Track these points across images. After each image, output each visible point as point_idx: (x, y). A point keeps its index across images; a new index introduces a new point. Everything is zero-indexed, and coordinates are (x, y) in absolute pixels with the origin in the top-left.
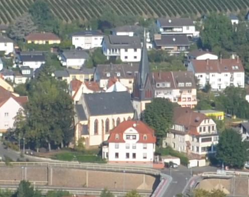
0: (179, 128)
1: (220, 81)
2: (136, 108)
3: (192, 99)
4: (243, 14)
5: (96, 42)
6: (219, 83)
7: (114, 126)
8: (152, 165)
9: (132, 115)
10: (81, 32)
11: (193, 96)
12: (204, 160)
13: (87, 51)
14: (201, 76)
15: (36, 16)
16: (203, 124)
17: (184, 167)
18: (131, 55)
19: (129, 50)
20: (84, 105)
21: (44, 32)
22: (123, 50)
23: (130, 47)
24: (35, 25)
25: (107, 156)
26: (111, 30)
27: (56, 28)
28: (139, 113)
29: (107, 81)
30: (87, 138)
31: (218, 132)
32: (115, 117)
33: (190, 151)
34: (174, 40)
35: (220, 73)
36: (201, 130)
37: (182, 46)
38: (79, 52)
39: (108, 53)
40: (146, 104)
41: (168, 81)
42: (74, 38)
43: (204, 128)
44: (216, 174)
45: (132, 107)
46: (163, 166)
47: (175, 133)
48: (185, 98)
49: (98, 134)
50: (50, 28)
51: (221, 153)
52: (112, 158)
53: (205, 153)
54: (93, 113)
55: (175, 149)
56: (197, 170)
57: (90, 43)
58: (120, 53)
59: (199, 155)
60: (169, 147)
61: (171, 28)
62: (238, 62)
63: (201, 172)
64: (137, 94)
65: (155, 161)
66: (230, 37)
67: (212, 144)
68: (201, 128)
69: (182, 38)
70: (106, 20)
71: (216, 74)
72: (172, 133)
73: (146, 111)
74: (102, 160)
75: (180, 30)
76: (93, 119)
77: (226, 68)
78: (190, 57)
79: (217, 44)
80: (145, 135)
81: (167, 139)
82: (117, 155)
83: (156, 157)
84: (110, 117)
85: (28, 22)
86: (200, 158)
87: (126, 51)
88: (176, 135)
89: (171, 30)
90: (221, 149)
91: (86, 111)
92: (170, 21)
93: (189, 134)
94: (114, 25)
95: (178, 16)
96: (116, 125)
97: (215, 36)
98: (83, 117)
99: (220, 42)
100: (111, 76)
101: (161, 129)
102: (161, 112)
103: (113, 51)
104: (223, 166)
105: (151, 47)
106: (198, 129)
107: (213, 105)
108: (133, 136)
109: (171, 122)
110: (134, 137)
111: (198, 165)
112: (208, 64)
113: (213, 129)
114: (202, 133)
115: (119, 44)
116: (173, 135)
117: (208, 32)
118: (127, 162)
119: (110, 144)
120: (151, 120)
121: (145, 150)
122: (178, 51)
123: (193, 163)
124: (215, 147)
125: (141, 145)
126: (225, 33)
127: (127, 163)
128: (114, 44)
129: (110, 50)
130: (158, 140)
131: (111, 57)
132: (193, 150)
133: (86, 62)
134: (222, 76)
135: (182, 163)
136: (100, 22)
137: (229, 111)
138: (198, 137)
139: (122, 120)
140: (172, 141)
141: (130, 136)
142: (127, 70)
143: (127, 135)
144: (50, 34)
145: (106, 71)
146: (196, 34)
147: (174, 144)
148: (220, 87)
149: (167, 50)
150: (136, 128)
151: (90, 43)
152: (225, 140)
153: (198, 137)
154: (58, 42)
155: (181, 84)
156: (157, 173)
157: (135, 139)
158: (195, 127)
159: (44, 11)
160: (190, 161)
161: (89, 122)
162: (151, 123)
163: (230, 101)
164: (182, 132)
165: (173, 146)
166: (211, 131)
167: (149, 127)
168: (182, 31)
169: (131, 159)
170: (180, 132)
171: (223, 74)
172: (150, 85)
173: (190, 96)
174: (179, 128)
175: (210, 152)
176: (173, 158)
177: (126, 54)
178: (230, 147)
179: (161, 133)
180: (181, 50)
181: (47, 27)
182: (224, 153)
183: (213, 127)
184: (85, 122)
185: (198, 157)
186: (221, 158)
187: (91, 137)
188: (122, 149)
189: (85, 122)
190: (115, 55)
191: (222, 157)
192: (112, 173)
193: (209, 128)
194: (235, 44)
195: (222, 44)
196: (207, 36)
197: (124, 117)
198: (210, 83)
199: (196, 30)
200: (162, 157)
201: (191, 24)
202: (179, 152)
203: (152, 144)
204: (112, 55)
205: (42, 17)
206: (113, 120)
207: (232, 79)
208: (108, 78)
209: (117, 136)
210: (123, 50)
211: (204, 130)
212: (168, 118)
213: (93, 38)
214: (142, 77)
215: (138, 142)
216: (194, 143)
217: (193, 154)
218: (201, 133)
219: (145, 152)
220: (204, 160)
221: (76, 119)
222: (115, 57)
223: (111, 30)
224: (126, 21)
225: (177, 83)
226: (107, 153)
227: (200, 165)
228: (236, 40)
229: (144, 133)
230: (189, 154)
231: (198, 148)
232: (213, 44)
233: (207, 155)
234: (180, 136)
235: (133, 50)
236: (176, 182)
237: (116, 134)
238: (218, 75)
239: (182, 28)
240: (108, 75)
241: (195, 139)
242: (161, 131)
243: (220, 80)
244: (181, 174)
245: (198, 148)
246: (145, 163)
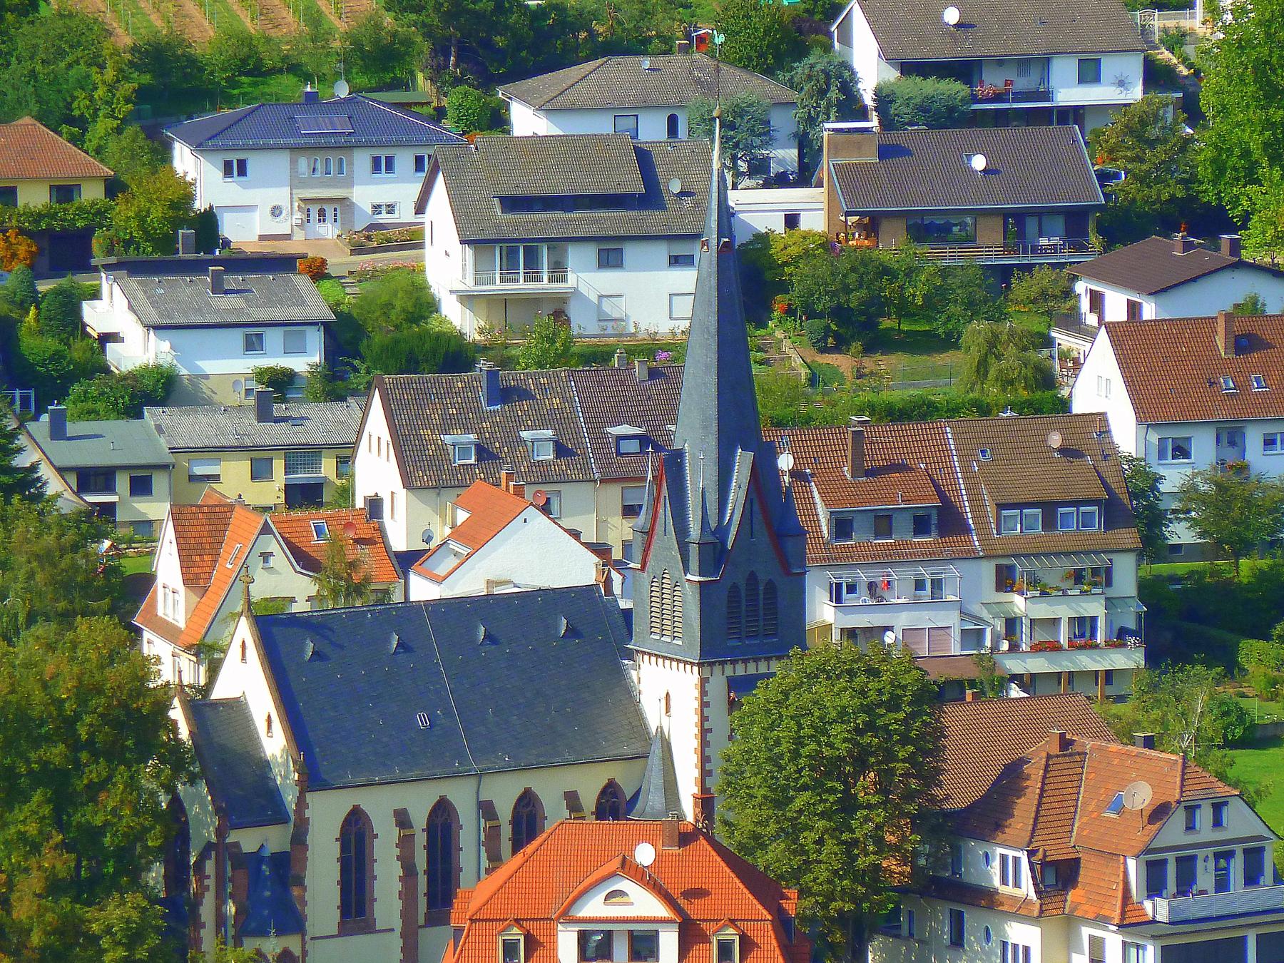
76: (326, 814)
161: (299, 839)
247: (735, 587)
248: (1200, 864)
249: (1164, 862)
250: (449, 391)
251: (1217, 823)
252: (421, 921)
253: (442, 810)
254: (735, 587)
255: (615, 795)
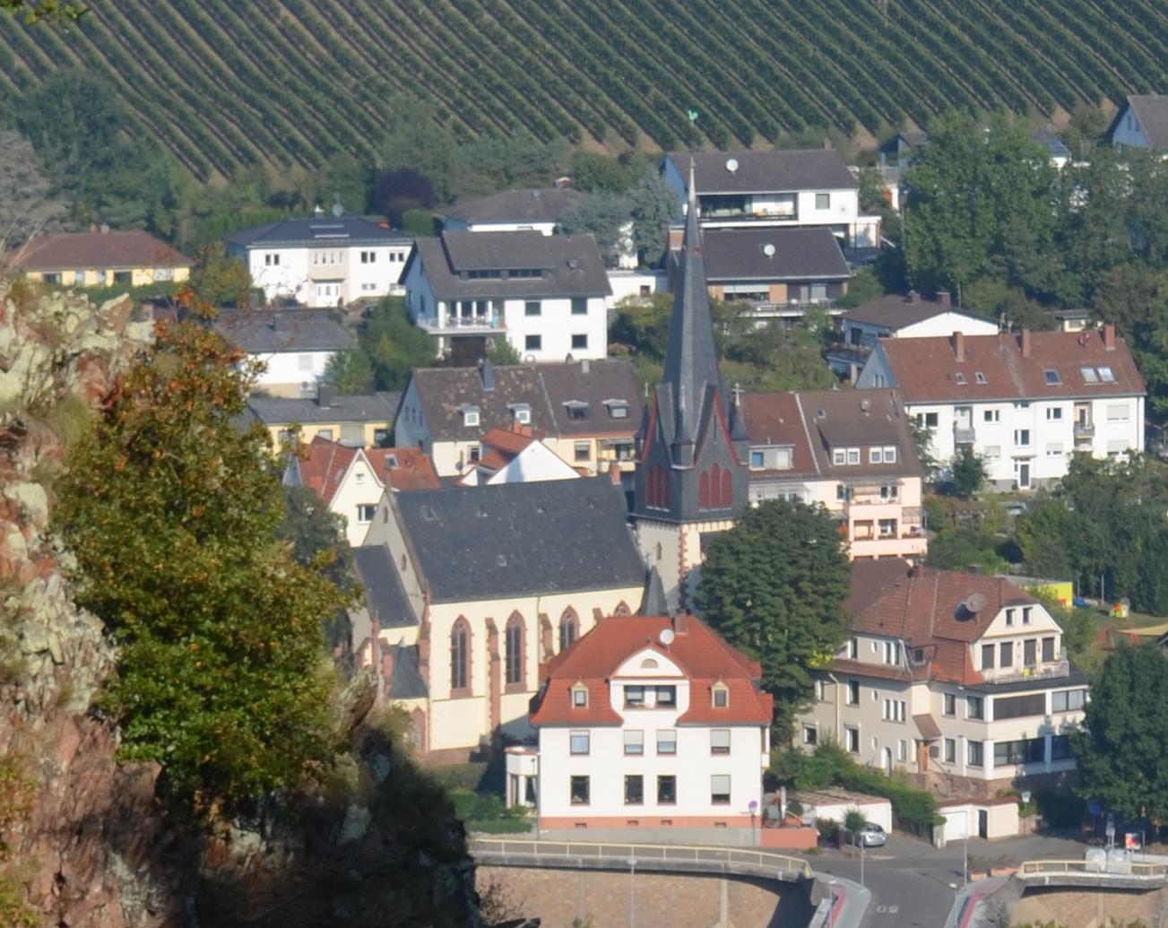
0: (874, 652)
1: (1027, 442)
2: (652, 561)
3: (903, 528)
4: (1084, 130)
5: (372, 272)
6: (1023, 451)
7: (549, 652)
8: (757, 835)
9: (632, 597)
10: (290, 222)
11: (907, 511)
12: (1013, 808)
13: (333, 315)
14: (932, 419)
15: (57, 151)
16: (998, 626)
17: (914, 844)
18: (558, 332)
19: (547, 305)
20: (398, 549)
21: (105, 229)
22: (514, 308)
23: (555, 294)
24: (51, 195)
25: (532, 795)
26: (439, 214)
27: (159, 207)
28: (670, 582)
29: (465, 447)
30: (418, 710)
31: (1073, 668)
32: (554, 605)
33: (936, 766)
34: (769, 250)
35: (1025, 404)
36: (988, 663)
37: (808, 283)
38: (292, 323)
39: (442, 323)
40: (705, 539)
41: (780, 438)
42: (257, 257)
43: (1007, 647)
44: (1081, 868)
45: (635, 556)
46: (811, 838)
47: (858, 678)
48: (869, 523)
49: (468, 694)
50: (130, 205)
51: (1102, 765)
52: (555, 802)
53: (1010, 772)
54: (445, 587)
55: (860, 760)
56: (982, 854)
57: (340, 281)
58: (502, 323)
59: (981, 785)
60: (828, 750)
61: (740, 202)
62: (1110, 348)
63: (1012, 862)
64: (655, 492)
65: (773, 811)
66: (1049, 237)
67: (1046, 729)
68: (988, 649)
69: (810, 250)
70: (405, 163)
71: (1006, 409)
72: (842, 677)
73: (711, 571)
74: (508, 815)
75: (787, 207)
76: (442, 616)
77: (1051, 376)
78: (856, 334)
79: (982, 271)
80: (720, 686)
81: (818, 707)
82: (580, 788)
83: (771, 796)
84: (528, 607)
85: (21, 177)
86: (991, 795)
87: (533, 309)
88: (862, 689)
89: (736, 211)
90: (1102, 746)
91: (409, 580)
92: (732, 165)
93: (933, 682)
94: (446, 194)
95: (761, 144)
96: (556, 649)
97: (972, 233)
98: (397, 612)
99: (999, 257)
100: (482, 425)
101: (790, 660)
102: (791, 571)
103: (467, 310)
104: (1111, 832)
105: (652, 289)
106: (976, 652)
107: (1010, 552)
108: (658, 689)
109: (838, 626)
110: (666, 696)
111: (983, 832)
112: (960, 359)
113: (1048, 656)
114: (998, 673)
115: (496, 274)
116: (848, 689)
117: (936, 210)
118: (634, 822)
119: (548, 736)
120: (739, 615)
121: (720, 759)
122: (790, 307)
123: (958, 823)
124: (1064, 744)
125: (697, 739)
126: (1023, 212)
127: (581, 830)
128: (472, 274)
129: (453, 311)
130: (777, 712)
131: (456, 340)
132: (951, 759)
133: (335, 368)
134: (1034, 415)
135: (900, 821)
136: (372, 176)
137: (1093, 579)
138: (976, 693)
139: (586, 624)
140: (831, 712)
141: (643, 689)
142: (564, 399)
143: (627, 689)
144: (138, 234)
145: (460, 399)
146: (867, 228)
147: (855, 734)
148: (1025, 469)
149: (736, 303)
150: (673, 652)
151: (340, 281)
152: (1122, 702)
153: (976, 693)
154: (181, 274)
155: (846, 455)
156: (787, 869)
157: (671, 704)
158: (963, 644)
159: (93, 126)
160: (946, 812)
161: (425, 634)
162: (738, 631)
163: (1083, 531)
164: (894, 671)
165: (848, 746)
166: (1041, 667)
167: (730, 647)
168: (795, 216)
169: (651, 806)
170: (881, 669)
171: (1040, 407)
172: (722, 439)
173: (892, 511)
174: (874, 652)
175: (1036, 769)
176: (858, 802)
177: (533, 325)
178: (1149, 733)
179: (792, 677)
180: (804, 301)
181: (116, 204)
182: (1115, 768)
183: (1048, 642)
184: (405, 636)
185: (979, 793)
186: (1105, 791)
187: (434, 706)
188: (606, 758)
189: (405, 636)
190: (475, 329)
191: (1109, 784)
192: (560, 874)
193: (1030, 645)
194: (1073, 267)
195: (1012, 268)
196: (929, 229)
197: (592, 606)
198: (978, 449)
199: (864, 209)
200: (799, 795)
201: (842, 182)
202: (877, 771)
203: (755, 732)
204: (461, 329)
205: (83, 155)
206: (544, 621)
207: (1083, 429)
208: (469, 434)
209: (580, 692)
210: (514, 308)
211: (1007, 661)
212: (821, 601)
213: (355, 252)
214: (683, 405)
215: (683, 721)
216: (958, 727)
217: (949, 778)
218: (988, 675)
219: (720, 772)
220: (1013, 808)
221: (361, 621)
222: (480, 339)
223: (439, 214)
224: (506, 170)
225: (827, 447)
226: (529, 780)
227: (992, 832)
228: (1077, 251)
229: (716, 678)
230: (933, 779)
231: (977, 747)
232: (961, 271)
233: (1019, 783)
234: (886, 694)
235: (566, 304)
236: (894, 910)
237: (575, 682)
238: (1012, 416)
239: (795, 198)
240: (472, 419)
241: (964, 707)
242: (790, 668)
243: (1025, 434)
244: (908, 871)
245: (977, 747)
246: (721, 823)
247: (705, 474)
248: (1015, 646)
249: (992, 646)
250: (460, 379)
251: (1026, 619)
252: (503, 690)
253: (516, 618)
254: (705, 474)
255: (624, 611)
